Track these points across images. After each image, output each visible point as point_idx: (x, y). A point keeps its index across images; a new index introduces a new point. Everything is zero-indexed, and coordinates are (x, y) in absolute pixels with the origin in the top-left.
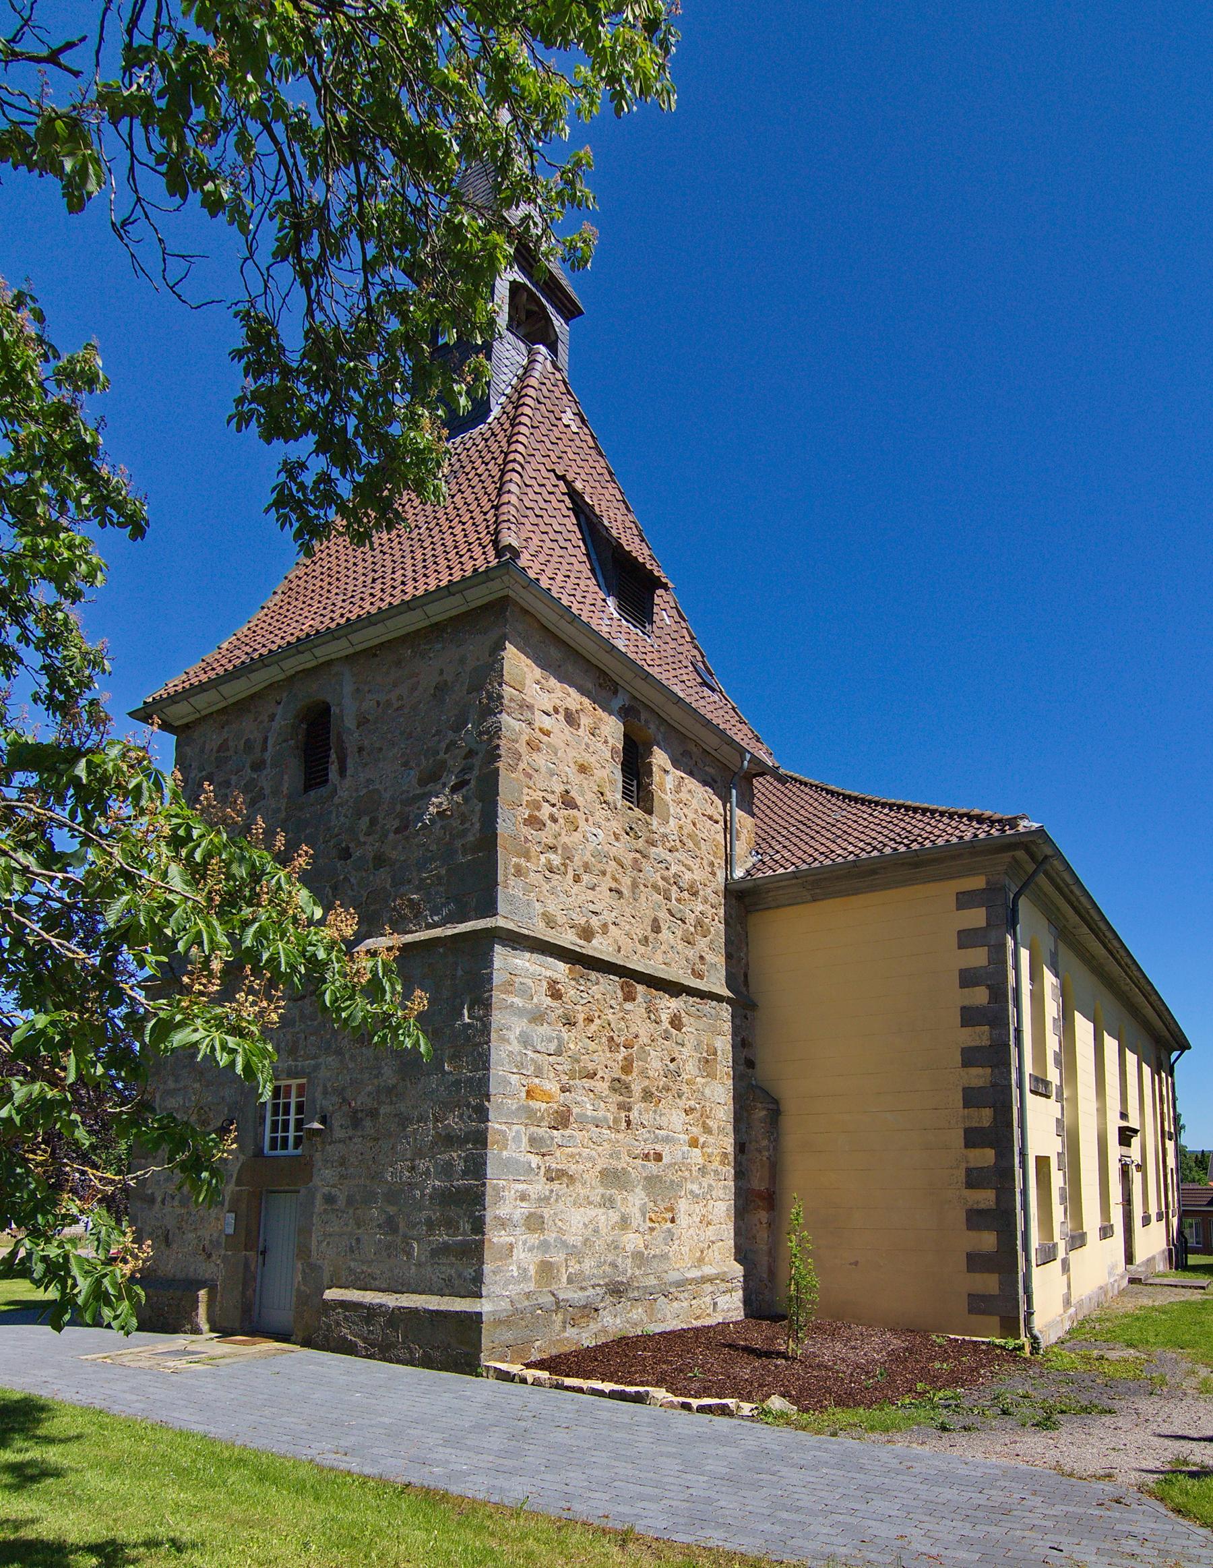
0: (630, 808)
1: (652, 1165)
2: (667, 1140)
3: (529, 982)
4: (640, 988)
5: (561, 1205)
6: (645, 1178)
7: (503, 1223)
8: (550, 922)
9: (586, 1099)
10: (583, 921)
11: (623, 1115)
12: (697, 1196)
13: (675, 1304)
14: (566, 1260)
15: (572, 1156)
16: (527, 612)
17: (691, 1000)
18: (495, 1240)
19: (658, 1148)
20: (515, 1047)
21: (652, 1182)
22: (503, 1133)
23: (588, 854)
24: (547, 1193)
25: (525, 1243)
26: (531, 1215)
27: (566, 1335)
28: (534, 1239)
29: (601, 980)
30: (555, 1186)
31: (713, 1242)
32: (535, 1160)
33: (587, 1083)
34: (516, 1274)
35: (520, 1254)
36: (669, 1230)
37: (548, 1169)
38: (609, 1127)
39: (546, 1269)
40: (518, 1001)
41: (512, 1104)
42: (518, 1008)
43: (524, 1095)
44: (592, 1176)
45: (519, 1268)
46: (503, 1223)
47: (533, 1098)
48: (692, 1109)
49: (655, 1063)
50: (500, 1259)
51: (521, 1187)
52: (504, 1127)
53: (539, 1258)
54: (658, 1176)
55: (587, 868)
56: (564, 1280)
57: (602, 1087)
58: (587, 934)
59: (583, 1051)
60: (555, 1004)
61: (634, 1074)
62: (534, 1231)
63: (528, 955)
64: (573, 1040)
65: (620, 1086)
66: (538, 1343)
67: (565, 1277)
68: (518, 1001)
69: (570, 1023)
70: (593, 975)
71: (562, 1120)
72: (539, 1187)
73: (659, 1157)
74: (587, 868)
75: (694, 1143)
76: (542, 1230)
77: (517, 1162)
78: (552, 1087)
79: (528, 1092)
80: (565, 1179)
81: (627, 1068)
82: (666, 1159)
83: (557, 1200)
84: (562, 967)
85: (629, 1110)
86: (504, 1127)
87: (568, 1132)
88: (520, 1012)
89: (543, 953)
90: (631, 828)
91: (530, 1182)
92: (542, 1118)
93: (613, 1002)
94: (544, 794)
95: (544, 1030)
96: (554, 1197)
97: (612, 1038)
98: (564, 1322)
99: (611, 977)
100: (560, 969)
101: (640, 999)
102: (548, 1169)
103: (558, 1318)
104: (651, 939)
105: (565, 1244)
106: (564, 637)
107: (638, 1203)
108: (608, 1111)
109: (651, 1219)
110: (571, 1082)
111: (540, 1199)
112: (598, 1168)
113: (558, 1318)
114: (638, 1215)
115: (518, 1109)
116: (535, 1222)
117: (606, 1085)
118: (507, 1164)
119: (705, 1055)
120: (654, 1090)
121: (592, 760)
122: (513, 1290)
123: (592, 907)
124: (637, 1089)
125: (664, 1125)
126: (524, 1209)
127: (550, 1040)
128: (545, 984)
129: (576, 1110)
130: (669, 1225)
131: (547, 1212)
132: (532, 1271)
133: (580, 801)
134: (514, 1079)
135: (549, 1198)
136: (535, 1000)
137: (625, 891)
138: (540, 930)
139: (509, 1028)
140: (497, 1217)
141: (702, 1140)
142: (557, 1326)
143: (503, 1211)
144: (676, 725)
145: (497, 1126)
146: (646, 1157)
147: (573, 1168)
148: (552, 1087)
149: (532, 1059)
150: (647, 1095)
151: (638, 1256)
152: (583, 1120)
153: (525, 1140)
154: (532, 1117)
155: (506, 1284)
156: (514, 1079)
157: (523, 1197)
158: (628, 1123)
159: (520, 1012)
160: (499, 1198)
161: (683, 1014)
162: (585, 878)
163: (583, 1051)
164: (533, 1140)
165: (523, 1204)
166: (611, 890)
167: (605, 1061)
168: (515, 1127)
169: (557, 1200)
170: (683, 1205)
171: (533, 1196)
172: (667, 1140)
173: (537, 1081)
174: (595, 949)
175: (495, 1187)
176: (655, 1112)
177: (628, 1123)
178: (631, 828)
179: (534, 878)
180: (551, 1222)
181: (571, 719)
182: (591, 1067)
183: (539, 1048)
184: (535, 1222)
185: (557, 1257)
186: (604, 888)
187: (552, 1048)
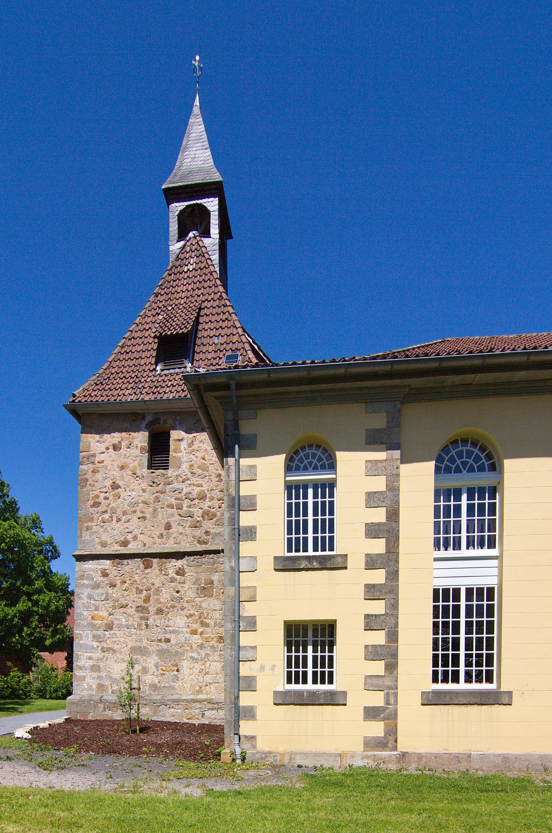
0: (152, 472)
1: (164, 645)
2: (173, 632)
3: (92, 573)
4: (155, 561)
5: (109, 662)
6: (158, 651)
7: (81, 668)
8: (104, 544)
9: (122, 617)
10: (122, 539)
11: (143, 622)
12: (196, 659)
13: (172, 710)
14: (111, 684)
15: (115, 642)
16: (90, 414)
17: (192, 558)
18: (77, 674)
19: (168, 636)
20: (86, 600)
21: (161, 653)
22: (81, 634)
23: (126, 506)
24: (102, 657)
25: (91, 676)
26: (93, 665)
27: (106, 713)
28: (95, 674)
29: (130, 562)
30: (106, 654)
31: (210, 683)
32: (95, 644)
33: (122, 610)
34: (86, 687)
35: (88, 680)
36: (175, 675)
37: (103, 648)
38: (135, 629)
39: (101, 687)
40: (86, 582)
41: (84, 623)
42: (86, 585)
43: (90, 618)
44: (126, 650)
45: (88, 685)
46: (81, 668)
47: (94, 620)
48: (191, 616)
49: (166, 595)
50: (80, 681)
51: (88, 654)
52: (81, 632)
53: (98, 682)
54: (167, 650)
55: (124, 513)
56: (110, 691)
57: (131, 611)
58: (125, 543)
59: (121, 596)
60: (105, 579)
61: (151, 603)
62: (95, 672)
63: (91, 562)
64: (114, 593)
65: (141, 609)
66: (91, 714)
67: (111, 691)
68: (86, 582)
69: (113, 586)
70: (125, 561)
71: (109, 627)
72: (98, 654)
73: (168, 641)
74: (124, 513)
75: (194, 632)
76: (99, 672)
77: (87, 645)
78: (104, 614)
79: (92, 617)
80: (111, 651)
81: (147, 600)
82: (173, 642)
83: (106, 660)
84: (108, 562)
85: (147, 619)
86: (81, 632)
87: (112, 632)
88: (87, 586)
89: (98, 559)
90: (154, 483)
91: (94, 653)
92: (99, 627)
93: (138, 571)
94: (99, 490)
95: (100, 591)
96: (105, 658)
97: (138, 588)
98: (104, 708)
99: (136, 560)
100: (107, 564)
101: (155, 565)
102: (103, 648)
103: (101, 706)
104: (164, 534)
105: (111, 678)
106: (109, 412)
107: (153, 662)
108: (135, 619)
109: (162, 670)
110: (114, 611)
111: (98, 659)
112: (129, 646)
113: (101, 706)
114: (154, 667)
115: (87, 624)
116: (95, 668)
117: (133, 610)
118: (81, 646)
119: (203, 585)
120: (164, 608)
121: (128, 461)
122: (85, 693)
123: (127, 530)
124: (152, 609)
125: (172, 624)
126: (90, 663)
127: (102, 595)
128: (100, 572)
129: (116, 622)
130: (175, 673)
131: (101, 665)
132: (94, 687)
133: (121, 483)
134: (85, 613)
135: (103, 659)
136: (95, 579)
137: (148, 516)
138: (100, 550)
139: (83, 593)
140: (78, 666)
141: (200, 631)
142: (101, 709)
143: (80, 663)
144: (187, 410)
145: (78, 632)
146: (160, 640)
147: (116, 647)
148: (104, 614)
149: (93, 604)
150: (160, 611)
151: (154, 687)
152: (120, 626)
153: (90, 636)
154: (94, 627)
155: (82, 690)
156: (85, 613)
157: (90, 658)
158: (147, 626)
159: (87, 586)
160: (78, 658)
161: (185, 567)
162: (124, 518)
163: (121, 596)
164: (94, 636)
165: (90, 661)
166: (139, 518)
167: (134, 599)
168: (86, 632)
169: (106, 660)
170: (185, 664)
171: (94, 658)
172: (173, 632)
173: (96, 612)
174: (130, 549)
175: (77, 655)
176: (165, 619)
177: (147, 626)
178: (154, 483)
179: (95, 529)
180: (103, 669)
181: (116, 448)
182: (124, 603)
183: (96, 599)
184: (95, 668)
185: (107, 683)
186: (135, 518)
187: (103, 598)
